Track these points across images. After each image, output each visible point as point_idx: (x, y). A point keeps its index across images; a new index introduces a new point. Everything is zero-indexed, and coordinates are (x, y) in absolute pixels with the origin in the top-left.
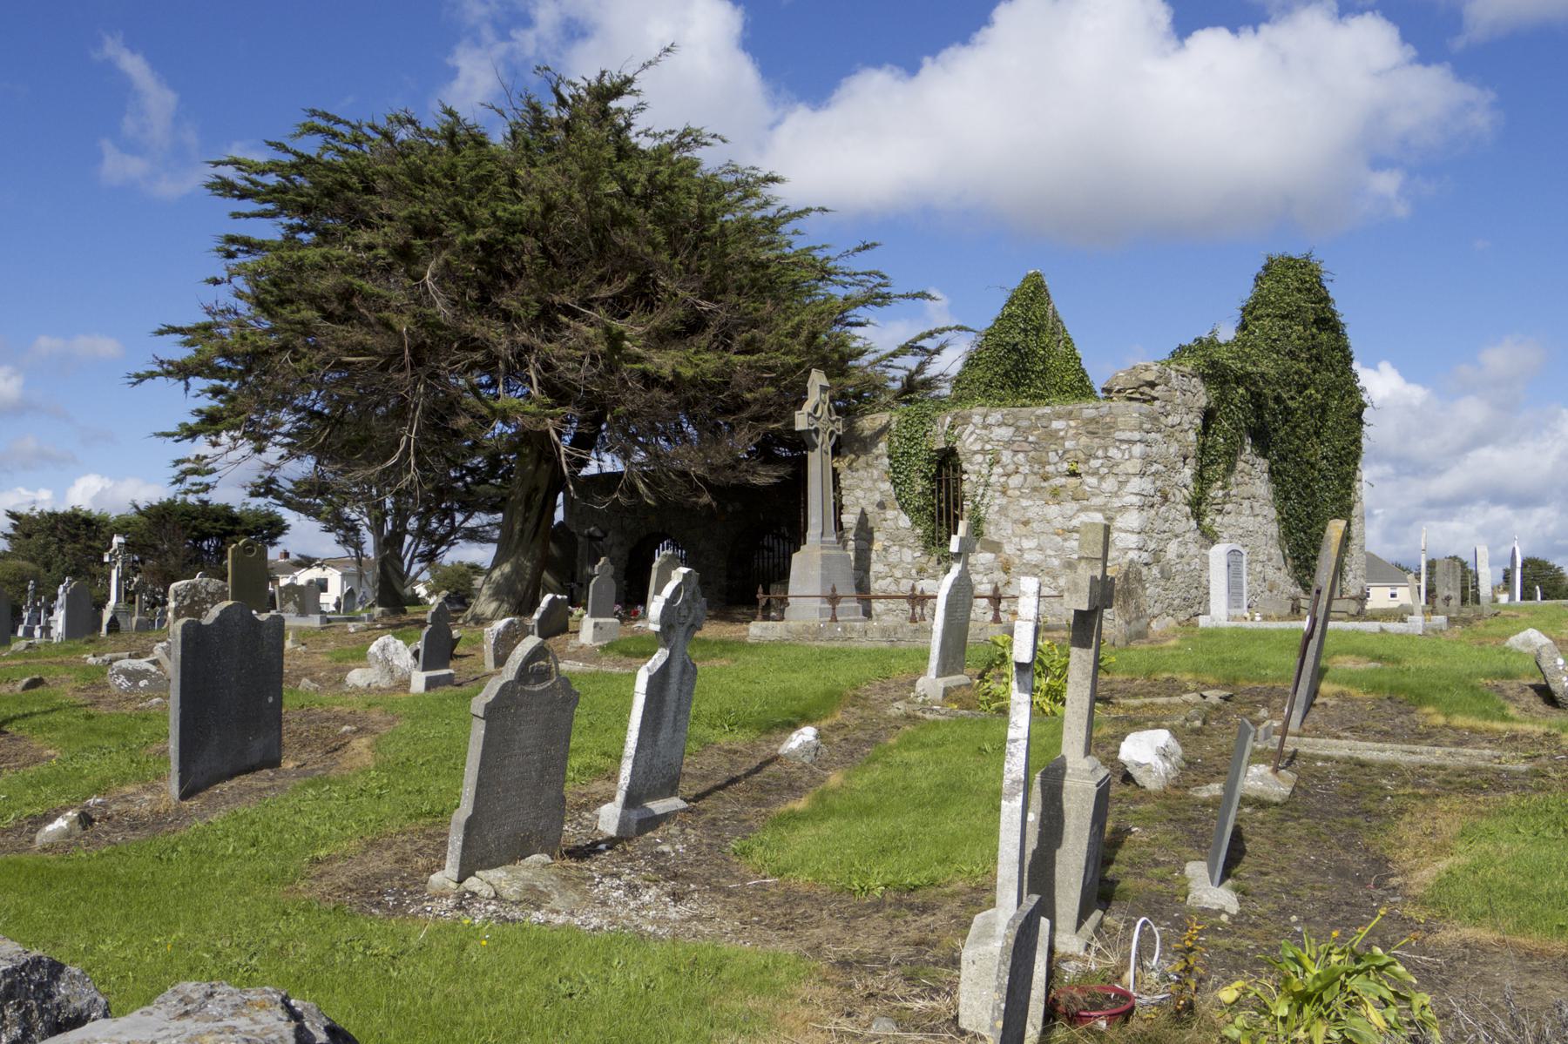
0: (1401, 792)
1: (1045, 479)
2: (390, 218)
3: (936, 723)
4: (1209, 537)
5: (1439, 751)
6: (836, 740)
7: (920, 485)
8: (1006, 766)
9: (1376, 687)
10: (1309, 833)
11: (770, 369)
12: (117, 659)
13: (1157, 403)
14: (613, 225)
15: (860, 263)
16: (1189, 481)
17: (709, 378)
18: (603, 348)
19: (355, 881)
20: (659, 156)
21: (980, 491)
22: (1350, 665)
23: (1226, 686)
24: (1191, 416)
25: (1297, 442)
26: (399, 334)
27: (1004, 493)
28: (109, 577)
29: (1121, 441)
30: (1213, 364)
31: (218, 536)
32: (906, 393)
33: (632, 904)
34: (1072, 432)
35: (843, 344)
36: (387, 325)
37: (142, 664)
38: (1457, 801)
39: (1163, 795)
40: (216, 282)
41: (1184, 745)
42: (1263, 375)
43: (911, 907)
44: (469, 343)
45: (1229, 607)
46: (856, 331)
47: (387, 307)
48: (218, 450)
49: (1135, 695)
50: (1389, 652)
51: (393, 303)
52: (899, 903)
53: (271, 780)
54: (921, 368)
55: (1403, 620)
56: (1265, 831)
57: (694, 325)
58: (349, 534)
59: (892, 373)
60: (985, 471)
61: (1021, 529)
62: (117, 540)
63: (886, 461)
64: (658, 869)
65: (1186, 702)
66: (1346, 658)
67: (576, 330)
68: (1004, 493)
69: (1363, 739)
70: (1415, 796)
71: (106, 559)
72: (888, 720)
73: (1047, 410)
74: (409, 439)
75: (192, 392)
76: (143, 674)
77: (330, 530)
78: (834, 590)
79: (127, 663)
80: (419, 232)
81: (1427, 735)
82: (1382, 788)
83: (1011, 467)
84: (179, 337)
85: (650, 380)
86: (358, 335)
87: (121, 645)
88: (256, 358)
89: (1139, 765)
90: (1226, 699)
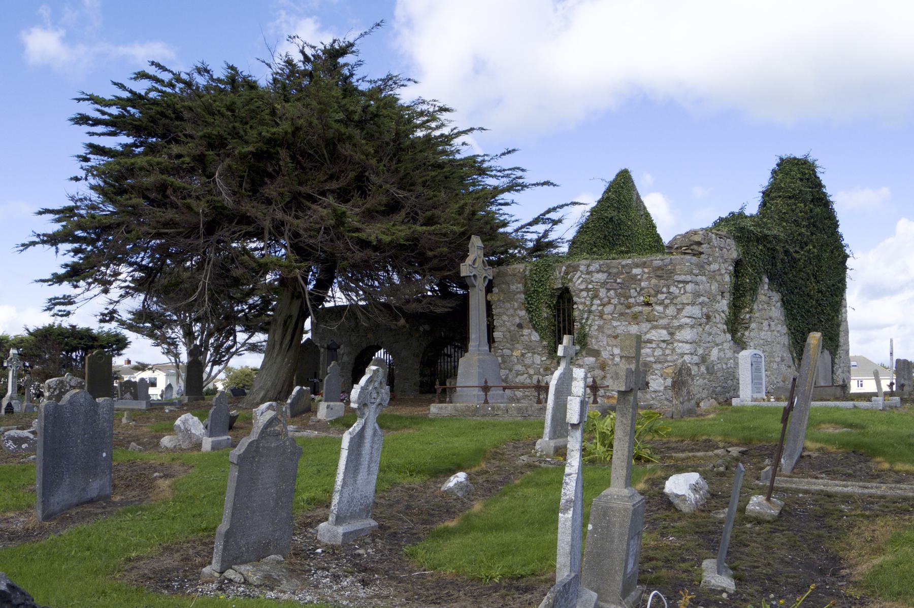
0: (853, 513)
1: (629, 307)
2: (191, 137)
3: (547, 469)
4: (740, 344)
5: (884, 487)
6: (481, 481)
7: (545, 312)
8: (563, 491)
9: (844, 445)
10: (789, 541)
11: (445, 235)
12: (9, 430)
13: (702, 256)
14: (339, 141)
15: (506, 163)
16: (726, 308)
17: (402, 242)
18: (332, 222)
19: (154, 573)
20: (373, 94)
21: (585, 316)
22: (831, 430)
23: (745, 444)
24: (726, 265)
25: (800, 281)
26: (197, 214)
27: (601, 317)
28: (7, 377)
29: (679, 282)
30: (742, 229)
31: (83, 349)
32: (537, 251)
33: (335, 587)
34: (646, 276)
35: (493, 219)
36: (189, 208)
37: (25, 433)
38: (890, 520)
39: (693, 516)
40: (77, 179)
41: (710, 484)
42: (775, 237)
43: (517, 589)
44: (245, 219)
45: (753, 392)
46: (505, 209)
47: (190, 196)
48: (78, 291)
49: (683, 451)
50: (857, 421)
51: (193, 194)
52: (509, 587)
53: (104, 508)
54: (546, 234)
55: (870, 401)
56: (759, 539)
57: (393, 207)
58: (171, 347)
59: (529, 236)
60: (588, 303)
61: (612, 341)
62: (13, 351)
63: (523, 296)
64: (355, 565)
65: (716, 455)
66: (828, 426)
67: (315, 211)
68: (601, 317)
69: (834, 479)
70: (862, 516)
71: (5, 365)
72: (516, 468)
73: (629, 261)
74: (204, 283)
75: (61, 252)
76: (25, 440)
77: (158, 345)
78: (486, 382)
79: (14, 433)
80: (210, 146)
81: (877, 476)
82: (841, 511)
83: (606, 300)
84: (51, 216)
85: (364, 244)
86: (170, 214)
87: (11, 422)
88: (103, 228)
89: (677, 496)
90: (743, 453)
